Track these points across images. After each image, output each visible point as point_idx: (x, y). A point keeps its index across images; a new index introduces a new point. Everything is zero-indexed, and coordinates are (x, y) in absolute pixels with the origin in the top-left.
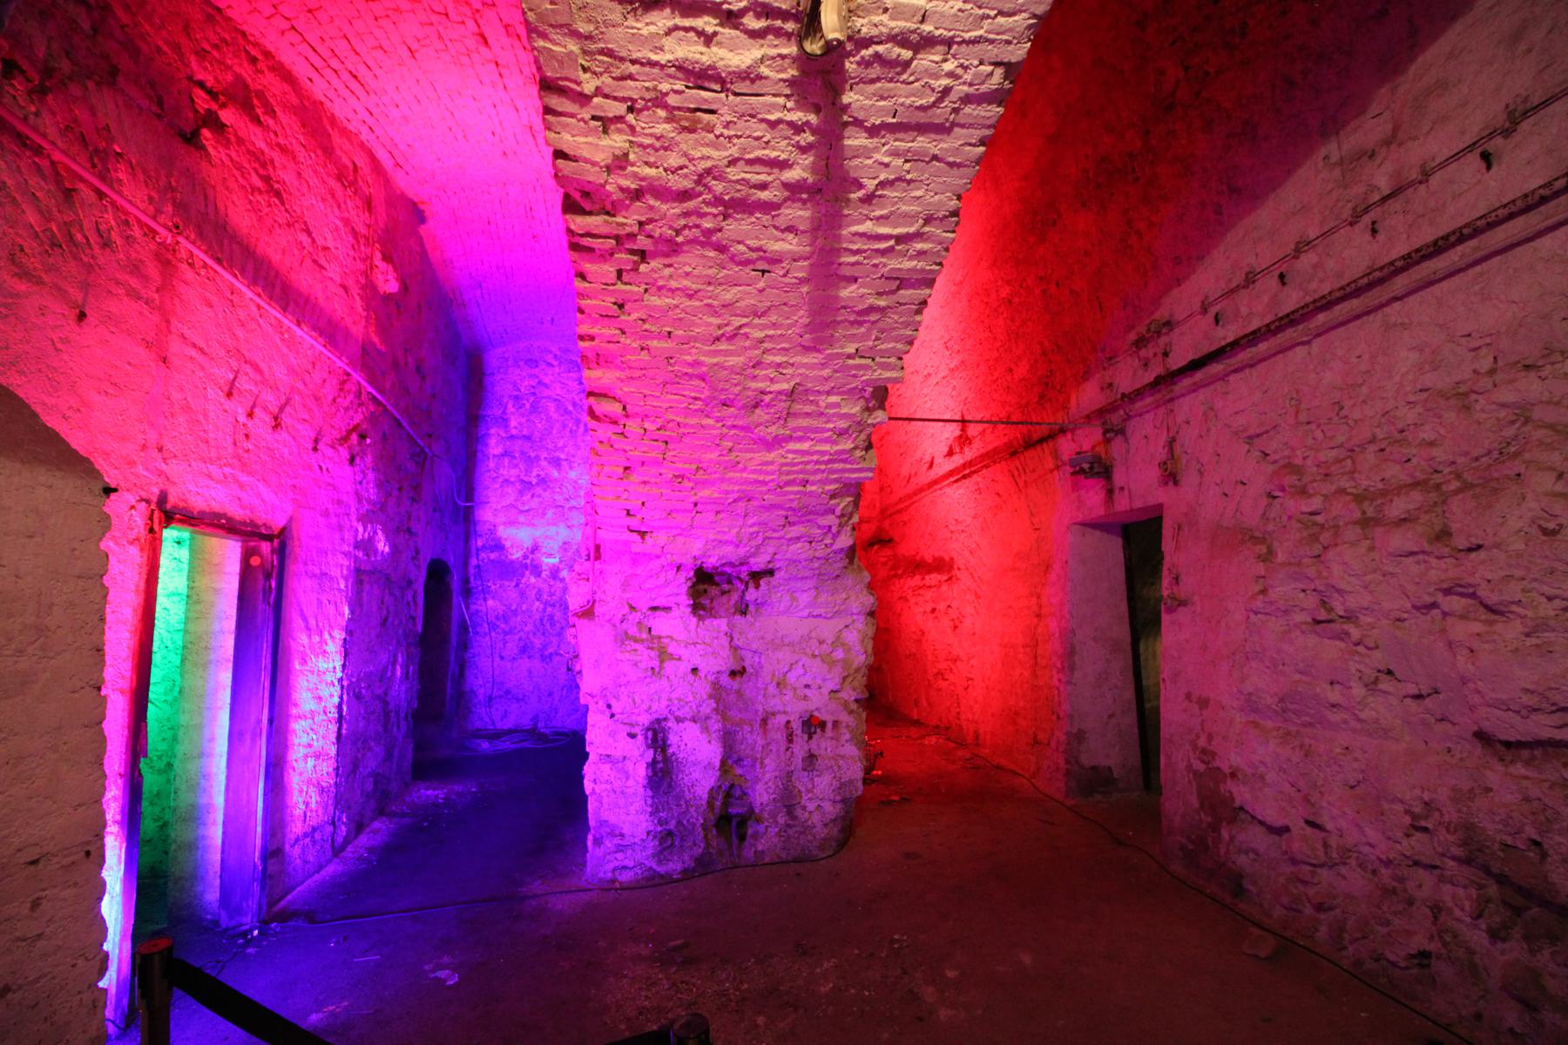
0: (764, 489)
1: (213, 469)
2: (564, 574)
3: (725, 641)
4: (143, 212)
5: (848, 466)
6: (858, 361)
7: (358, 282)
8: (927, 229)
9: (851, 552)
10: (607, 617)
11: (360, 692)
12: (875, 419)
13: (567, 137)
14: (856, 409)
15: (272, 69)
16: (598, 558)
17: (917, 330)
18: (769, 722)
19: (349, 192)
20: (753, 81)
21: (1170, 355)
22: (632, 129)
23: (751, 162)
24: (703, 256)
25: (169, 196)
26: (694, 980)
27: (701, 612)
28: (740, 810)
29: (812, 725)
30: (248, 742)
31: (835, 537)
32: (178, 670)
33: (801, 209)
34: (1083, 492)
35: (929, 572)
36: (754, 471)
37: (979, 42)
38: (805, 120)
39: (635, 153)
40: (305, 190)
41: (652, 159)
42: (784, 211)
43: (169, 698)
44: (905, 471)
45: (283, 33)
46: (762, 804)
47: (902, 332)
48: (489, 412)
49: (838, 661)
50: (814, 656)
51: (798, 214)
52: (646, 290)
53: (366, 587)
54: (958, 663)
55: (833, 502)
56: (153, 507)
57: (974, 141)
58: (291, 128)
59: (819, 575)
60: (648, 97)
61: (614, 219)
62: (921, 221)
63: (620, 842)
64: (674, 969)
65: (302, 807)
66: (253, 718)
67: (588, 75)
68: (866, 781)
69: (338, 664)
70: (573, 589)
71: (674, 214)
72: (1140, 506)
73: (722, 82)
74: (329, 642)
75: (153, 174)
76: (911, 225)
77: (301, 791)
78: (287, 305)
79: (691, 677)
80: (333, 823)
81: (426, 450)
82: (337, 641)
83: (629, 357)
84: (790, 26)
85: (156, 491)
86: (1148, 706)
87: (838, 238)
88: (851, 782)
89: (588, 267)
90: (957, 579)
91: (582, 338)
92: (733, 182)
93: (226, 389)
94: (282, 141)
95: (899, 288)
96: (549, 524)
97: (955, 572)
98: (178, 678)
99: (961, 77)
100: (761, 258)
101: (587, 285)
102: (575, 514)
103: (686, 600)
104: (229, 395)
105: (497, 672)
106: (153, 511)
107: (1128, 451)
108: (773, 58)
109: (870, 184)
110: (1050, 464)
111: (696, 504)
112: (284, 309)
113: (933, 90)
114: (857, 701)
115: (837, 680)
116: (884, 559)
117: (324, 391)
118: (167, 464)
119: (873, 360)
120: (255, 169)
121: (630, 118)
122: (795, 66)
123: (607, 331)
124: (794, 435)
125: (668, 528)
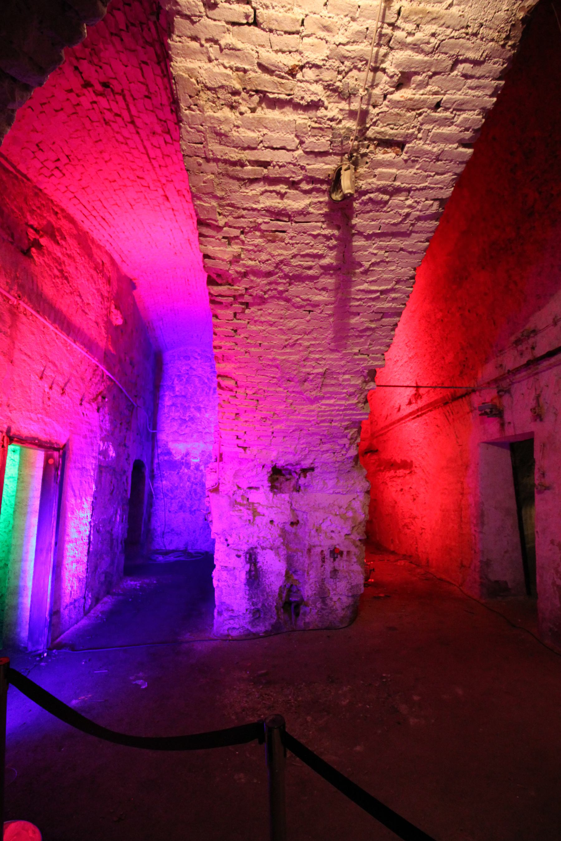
0: (309, 424)
1: (33, 415)
2: (202, 467)
3: (288, 506)
4: (4, 290)
5: (355, 412)
6: (360, 356)
7: (103, 320)
8: (397, 286)
9: (356, 459)
10: (226, 492)
11: (99, 529)
12: (369, 386)
13: (210, 247)
14: (359, 382)
15: (65, 217)
16: (221, 460)
17: (392, 339)
18: (312, 551)
19: (100, 275)
20: (305, 215)
21: (536, 349)
22: (243, 242)
23: (303, 256)
24: (278, 304)
25: (16, 281)
26: (272, 694)
27: (275, 490)
28: (296, 599)
29: (335, 553)
30: (45, 554)
31: (348, 450)
32: (12, 516)
33: (330, 279)
34: (486, 425)
35: (399, 469)
36: (304, 415)
37: (425, 189)
38: (332, 233)
39: (244, 254)
40: (79, 275)
41: (253, 257)
42: (321, 280)
43: (7, 530)
44: (384, 413)
45: (70, 199)
46: (308, 596)
47: (384, 340)
48: (165, 384)
49: (349, 518)
50: (337, 515)
51: (329, 281)
52: (248, 323)
53: (104, 474)
54: (416, 520)
55: (347, 431)
56: (4, 434)
57: (423, 240)
58: (73, 246)
59: (339, 470)
60: (251, 226)
61: (233, 287)
62: (394, 283)
63: (232, 614)
64: (261, 686)
65: (70, 588)
66: (47, 542)
67: (221, 217)
68: (366, 585)
69: (89, 514)
70: (208, 477)
71: (264, 284)
72: (520, 433)
73: (289, 216)
74: (85, 503)
75: (9, 271)
76: (389, 284)
77: (69, 580)
78: (70, 332)
79: (270, 525)
80: (84, 598)
81: (134, 404)
82: (89, 502)
83: (239, 357)
84: (324, 187)
85: (6, 426)
86: (528, 546)
87: (349, 293)
88: (357, 585)
89: (219, 312)
90: (415, 473)
91: (215, 347)
92: (294, 266)
93: (40, 375)
94: (69, 252)
95: (382, 318)
96: (195, 441)
97: (414, 469)
98: (12, 522)
99: (415, 208)
100: (308, 304)
101: (218, 321)
102: (208, 436)
103: (267, 484)
104: (41, 378)
105: (167, 519)
106: (4, 437)
107: (512, 402)
108: (315, 203)
109: (367, 265)
110: (467, 409)
111: (273, 433)
112: (68, 335)
113: (400, 215)
114: (360, 540)
115: (349, 528)
116: (374, 461)
117: (86, 375)
118: (11, 413)
119: (368, 355)
120: (56, 267)
121: (242, 237)
122: (327, 207)
123: (228, 344)
124: (326, 396)
125: (258, 445)
